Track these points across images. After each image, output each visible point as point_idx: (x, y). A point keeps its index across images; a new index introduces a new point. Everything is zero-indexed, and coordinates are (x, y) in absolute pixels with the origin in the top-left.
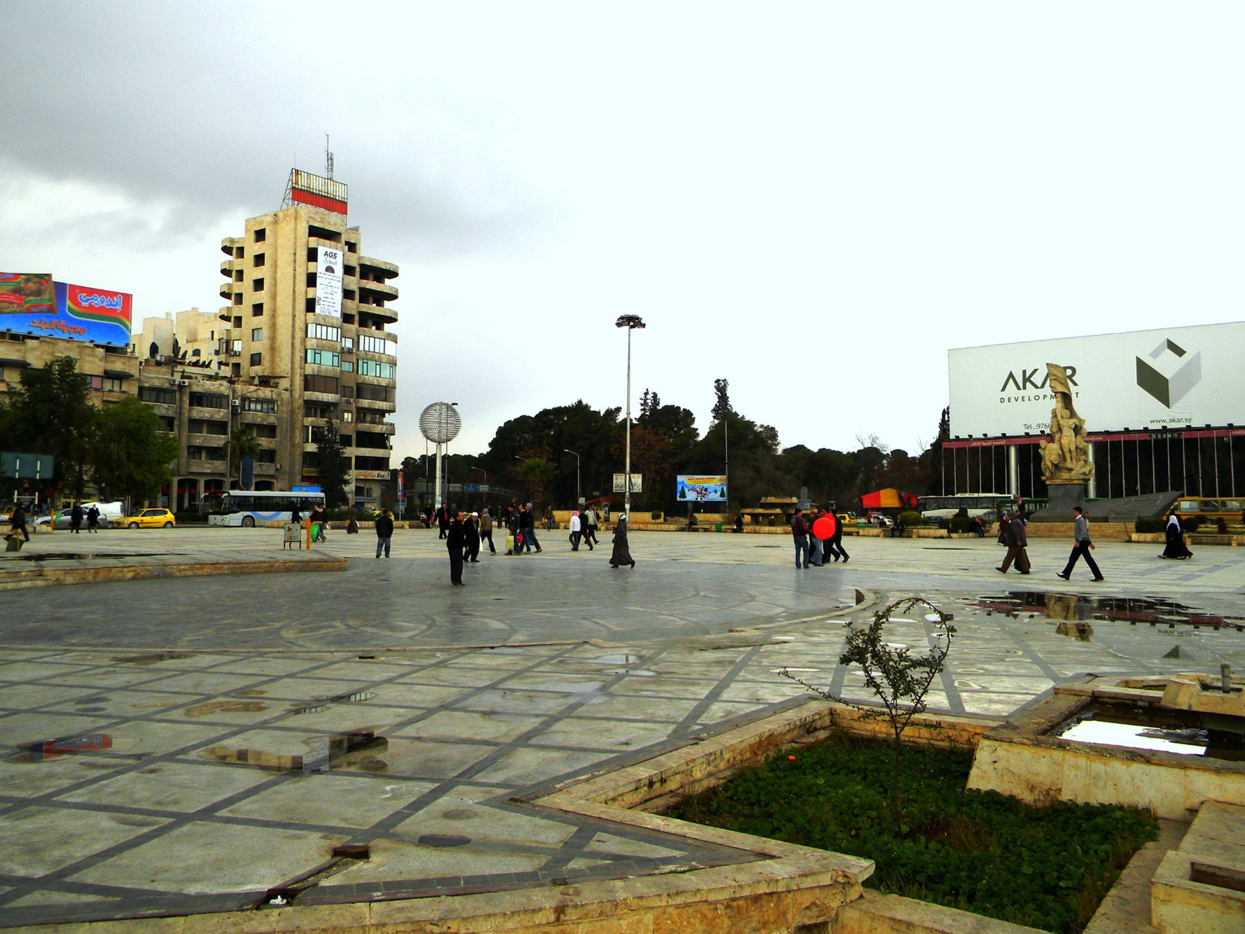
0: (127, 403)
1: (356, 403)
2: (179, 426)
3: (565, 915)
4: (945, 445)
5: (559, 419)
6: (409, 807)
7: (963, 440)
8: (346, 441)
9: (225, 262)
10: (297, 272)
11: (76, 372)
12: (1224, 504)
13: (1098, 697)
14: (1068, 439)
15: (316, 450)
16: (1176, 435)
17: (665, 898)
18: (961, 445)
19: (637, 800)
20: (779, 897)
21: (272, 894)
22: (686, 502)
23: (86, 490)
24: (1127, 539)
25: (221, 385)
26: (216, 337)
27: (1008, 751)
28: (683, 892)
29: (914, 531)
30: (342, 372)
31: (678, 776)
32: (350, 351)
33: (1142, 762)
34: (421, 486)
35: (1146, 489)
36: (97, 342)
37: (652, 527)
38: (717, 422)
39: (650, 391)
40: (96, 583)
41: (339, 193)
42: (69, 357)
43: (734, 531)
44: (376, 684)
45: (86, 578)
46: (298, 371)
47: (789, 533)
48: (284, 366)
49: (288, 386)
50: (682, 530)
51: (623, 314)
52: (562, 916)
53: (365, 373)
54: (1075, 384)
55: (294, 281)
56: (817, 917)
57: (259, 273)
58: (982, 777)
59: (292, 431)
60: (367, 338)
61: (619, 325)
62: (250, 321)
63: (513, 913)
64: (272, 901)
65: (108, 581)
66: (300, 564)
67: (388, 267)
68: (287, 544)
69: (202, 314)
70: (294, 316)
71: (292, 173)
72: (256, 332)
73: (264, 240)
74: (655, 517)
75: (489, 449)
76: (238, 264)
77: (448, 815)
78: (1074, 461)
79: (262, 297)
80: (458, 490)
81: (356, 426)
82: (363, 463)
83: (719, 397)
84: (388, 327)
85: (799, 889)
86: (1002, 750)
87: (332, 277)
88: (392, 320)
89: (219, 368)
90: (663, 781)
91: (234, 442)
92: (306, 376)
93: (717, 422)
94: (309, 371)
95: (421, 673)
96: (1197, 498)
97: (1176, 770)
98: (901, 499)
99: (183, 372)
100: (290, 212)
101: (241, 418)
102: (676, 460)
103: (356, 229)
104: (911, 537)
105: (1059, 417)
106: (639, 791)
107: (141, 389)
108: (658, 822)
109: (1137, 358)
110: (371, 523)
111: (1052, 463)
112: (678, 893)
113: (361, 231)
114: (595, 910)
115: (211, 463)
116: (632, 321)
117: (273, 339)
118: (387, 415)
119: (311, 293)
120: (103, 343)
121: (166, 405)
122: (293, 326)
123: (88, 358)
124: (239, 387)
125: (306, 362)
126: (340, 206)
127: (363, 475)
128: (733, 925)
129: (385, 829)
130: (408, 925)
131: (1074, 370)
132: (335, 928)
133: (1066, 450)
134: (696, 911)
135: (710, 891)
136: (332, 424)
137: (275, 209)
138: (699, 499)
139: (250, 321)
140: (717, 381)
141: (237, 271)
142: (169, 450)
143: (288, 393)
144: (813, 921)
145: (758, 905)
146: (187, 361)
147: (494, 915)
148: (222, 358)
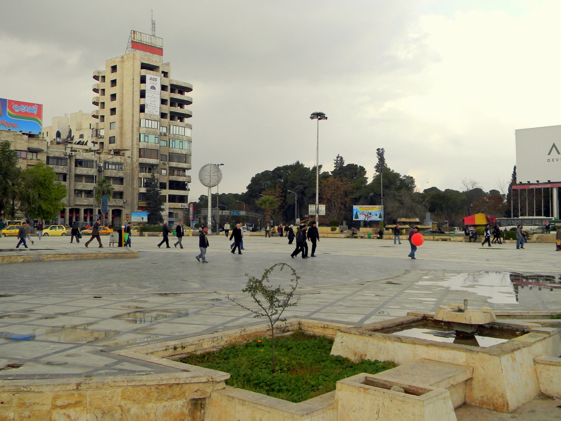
0: (38, 166)
3: (81, 387)
4: (514, 187)
8: (163, 186)
9: (95, 85)
10: (134, 89)
11: (11, 149)
15: (145, 192)
17: (126, 382)
19: (167, 355)
22: (360, 221)
23: (16, 215)
27: (347, 337)
31: (193, 346)
32: (165, 135)
33: (399, 342)
34: (203, 211)
36: (24, 132)
38: (378, 174)
41: (157, 43)
43: (378, 238)
44: (90, 308)
46: (135, 146)
47: (196, 235)
48: (127, 144)
49: (130, 155)
50: (348, 237)
52: (79, 387)
53: (174, 147)
55: (133, 95)
56: (201, 395)
57: (113, 90)
58: (335, 351)
59: (133, 180)
61: (312, 118)
62: (109, 118)
63: (58, 385)
65: (9, 263)
70: (133, 115)
73: (116, 72)
74: (333, 230)
75: (247, 190)
76: (102, 86)
77: (68, 356)
80: (228, 214)
81: (169, 177)
82: (173, 199)
83: (379, 159)
84: (186, 120)
86: (346, 337)
89: (94, 146)
90: (183, 347)
91: (99, 188)
92: (140, 149)
93: (378, 174)
94: (141, 147)
97: (412, 345)
98: (488, 220)
99: (72, 148)
101: (104, 173)
102: (353, 197)
103: (168, 64)
106: (167, 351)
107: (48, 158)
112: (132, 381)
113: (170, 65)
114: (94, 386)
115: (87, 200)
116: (320, 116)
117: (121, 128)
118: (186, 171)
119: (143, 101)
120: (28, 132)
122: (133, 120)
123: (19, 141)
124: (103, 156)
125: (140, 141)
126: (158, 51)
127: (173, 206)
128: (159, 396)
129: (36, 360)
130: (14, 387)
135: (147, 381)
136: (154, 177)
137: (122, 54)
138: (366, 219)
139: (109, 118)
140: (378, 149)
142: (63, 192)
143: (130, 159)
145: (172, 389)
146: (74, 141)
147: (50, 385)
148: (94, 139)
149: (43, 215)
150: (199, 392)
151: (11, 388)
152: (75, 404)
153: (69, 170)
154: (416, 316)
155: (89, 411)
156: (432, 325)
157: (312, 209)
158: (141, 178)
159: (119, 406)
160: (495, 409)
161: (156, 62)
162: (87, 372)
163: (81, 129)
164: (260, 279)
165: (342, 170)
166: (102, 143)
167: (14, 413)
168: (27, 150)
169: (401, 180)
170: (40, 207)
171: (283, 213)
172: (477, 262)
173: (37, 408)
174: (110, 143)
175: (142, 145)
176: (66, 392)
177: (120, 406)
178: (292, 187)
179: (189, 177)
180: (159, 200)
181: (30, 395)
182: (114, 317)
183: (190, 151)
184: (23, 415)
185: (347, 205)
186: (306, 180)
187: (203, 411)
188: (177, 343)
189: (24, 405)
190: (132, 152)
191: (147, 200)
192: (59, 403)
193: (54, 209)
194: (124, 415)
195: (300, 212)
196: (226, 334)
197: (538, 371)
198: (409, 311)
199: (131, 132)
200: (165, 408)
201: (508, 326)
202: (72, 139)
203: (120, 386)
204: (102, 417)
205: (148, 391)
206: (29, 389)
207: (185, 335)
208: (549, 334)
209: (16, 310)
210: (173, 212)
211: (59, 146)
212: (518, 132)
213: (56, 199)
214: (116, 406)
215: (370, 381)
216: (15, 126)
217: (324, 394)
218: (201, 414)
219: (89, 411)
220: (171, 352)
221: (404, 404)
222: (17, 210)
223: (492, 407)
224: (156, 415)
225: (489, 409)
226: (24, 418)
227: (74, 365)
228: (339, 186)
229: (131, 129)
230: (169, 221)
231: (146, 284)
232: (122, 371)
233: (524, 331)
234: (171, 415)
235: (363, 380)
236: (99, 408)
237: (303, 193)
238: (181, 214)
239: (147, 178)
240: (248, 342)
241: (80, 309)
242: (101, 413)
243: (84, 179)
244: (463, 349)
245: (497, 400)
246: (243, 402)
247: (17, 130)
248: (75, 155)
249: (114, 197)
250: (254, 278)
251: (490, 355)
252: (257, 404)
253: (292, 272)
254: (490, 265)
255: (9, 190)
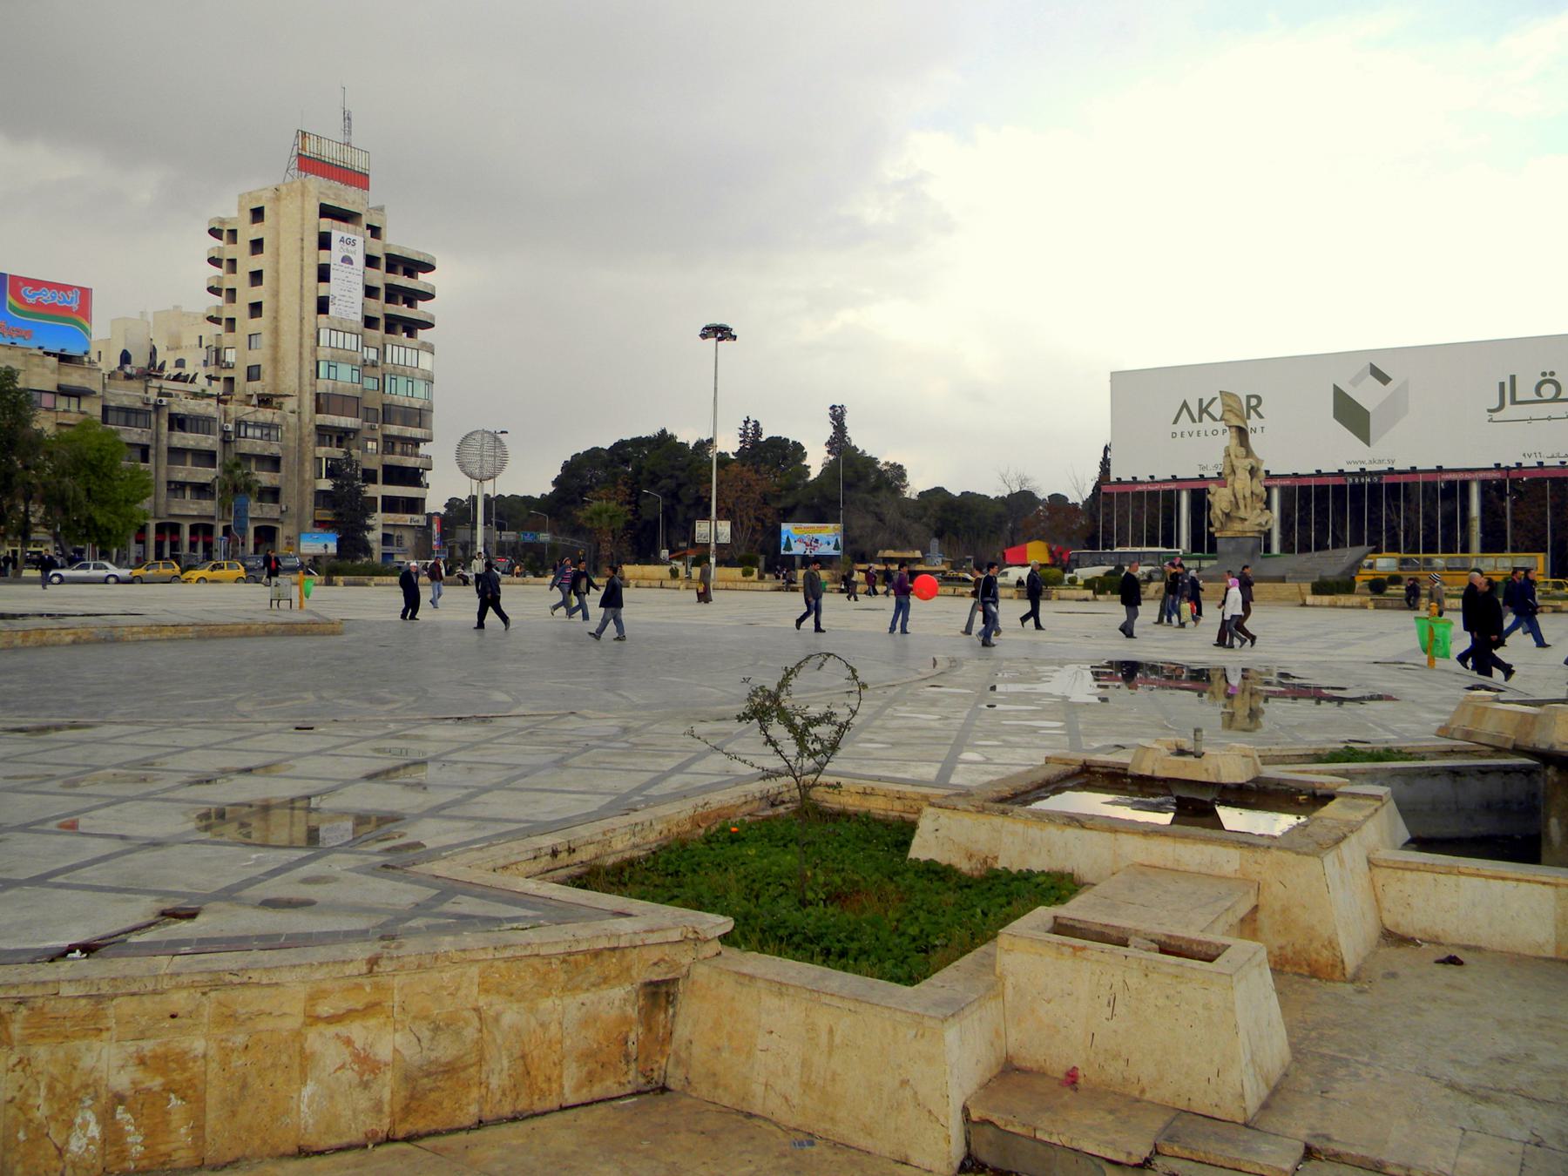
0: (85, 426)
1: (382, 429)
2: (156, 456)
3: (379, 967)
4: (1105, 489)
5: (639, 453)
6: (266, 874)
7: (1126, 483)
8: (370, 477)
9: (213, 249)
11: (19, 386)
12: (1428, 561)
13: (1088, 767)
14: (1243, 483)
15: (330, 488)
16: (1376, 479)
17: (491, 951)
18: (1122, 489)
20: (623, 953)
21: (71, 949)
22: (793, 556)
23: (33, 536)
24: (1301, 602)
25: (209, 405)
26: (204, 344)
27: (949, 818)
28: (511, 946)
29: (1054, 591)
30: (364, 390)
31: (592, 846)
32: (374, 365)
33: (1076, 827)
34: (462, 534)
35: (1338, 543)
36: (47, 349)
37: (742, 586)
38: (831, 458)
39: (752, 419)
40: (26, 648)
41: (358, 162)
42: (8, 367)
44: (300, 756)
45: (12, 642)
46: (307, 388)
48: (289, 383)
49: (296, 408)
50: (779, 589)
51: (708, 323)
52: (375, 967)
53: (393, 392)
54: (1261, 417)
55: (302, 274)
56: (667, 973)
57: (256, 263)
58: (921, 849)
59: (301, 463)
60: (395, 348)
61: (704, 336)
62: (246, 324)
63: (321, 964)
64: (70, 955)
65: (40, 646)
66: (283, 627)
67: (421, 258)
68: (275, 603)
69: (187, 315)
70: (302, 320)
71: (298, 136)
72: (253, 338)
73: (263, 220)
75: (552, 489)
76: (229, 251)
77: (307, 881)
78: (1249, 509)
79: (260, 294)
80: (512, 539)
81: (383, 458)
82: (391, 504)
85: (645, 945)
86: (945, 817)
87: (350, 270)
88: (428, 325)
89: (210, 384)
90: (571, 851)
91: (226, 477)
92: (318, 395)
93: (831, 458)
94: (321, 389)
95: (359, 745)
96: (1396, 554)
97: (1108, 834)
98: (1052, 554)
99: (160, 388)
100: (295, 186)
102: (780, 506)
103: (381, 209)
104: (1050, 599)
105: (1233, 456)
106: (538, 860)
107: (105, 409)
108: (531, 886)
109: (1335, 386)
110: (396, 579)
111: (1223, 513)
112: (505, 947)
113: (386, 211)
115: (198, 503)
116: (720, 332)
117: (275, 347)
119: (323, 289)
120: (57, 350)
121: (139, 430)
122: (301, 330)
123: (36, 369)
124: (233, 408)
125: (317, 377)
126: (359, 179)
128: (570, 979)
129: (229, 895)
130: (205, 975)
131: (1259, 399)
132: (125, 977)
133: (1240, 496)
134: (528, 965)
135: (542, 945)
136: (351, 456)
138: (808, 553)
139: (246, 324)
140: (833, 407)
141: (228, 260)
142: (143, 487)
143: (295, 416)
144: (660, 978)
145: (599, 961)
146: (166, 374)
147: (300, 965)
148: (212, 370)
149: (97, 535)
150: (663, 965)
151: (198, 978)
152: (365, 1009)
153: (154, 437)
154: (1066, 764)
155: (398, 1026)
156: (1106, 782)
157: (702, 529)
158: (320, 459)
159: (474, 1010)
160: (1314, 974)
161: (354, 202)
162: (380, 926)
163: (178, 348)
164: (772, 687)
165: (757, 450)
166: (230, 380)
167: (207, 1041)
168: (55, 390)
169: (879, 471)
170: (90, 519)
171: (630, 538)
172: (1067, 640)
173: (264, 1024)
174: (248, 380)
175: (323, 386)
176: (341, 982)
177: (477, 1010)
178: (652, 483)
179: (429, 457)
180: (362, 507)
181: (249, 993)
182: (371, 777)
183: (430, 403)
184: (230, 1044)
185: (768, 523)
186: (683, 470)
187: (671, 1011)
188: (560, 841)
189: (232, 1020)
190: (300, 400)
191: (334, 507)
192: (324, 1009)
193: (124, 525)
194: (485, 1031)
195: (667, 536)
196: (660, 814)
197: (1379, 885)
198: (1049, 753)
199: (297, 356)
200: (584, 1009)
201: (1279, 784)
202: (162, 368)
203: (478, 961)
204: (433, 1039)
205: (543, 969)
206: (245, 979)
207: (566, 820)
208: (1381, 800)
209: (115, 762)
210: (391, 533)
211: (129, 383)
212: (1117, 378)
213: (127, 501)
214: (467, 1009)
215: (1066, 925)
216: (27, 335)
217: (960, 960)
218: (666, 1017)
219: (398, 1026)
220: (545, 862)
221: (1181, 983)
222: (36, 525)
223: (1305, 970)
224: (561, 1028)
225: (1301, 975)
226: (233, 1050)
227: (334, 908)
228: (752, 483)
229: (298, 350)
230: (383, 554)
231: (383, 693)
232: (465, 921)
233: (1314, 794)
234: (598, 1025)
235: (1050, 924)
236: (425, 1018)
237: (673, 496)
238: (409, 539)
239: (332, 459)
240: (709, 833)
241: (276, 757)
242: (428, 1029)
243: (189, 459)
244: (1232, 842)
245: (1318, 954)
246: (780, 988)
247: (32, 344)
248: (169, 405)
249: (260, 499)
250: (762, 688)
251: (1298, 853)
252: (818, 992)
253: (849, 673)
254: (1099, 648)
255: (17, 479)
